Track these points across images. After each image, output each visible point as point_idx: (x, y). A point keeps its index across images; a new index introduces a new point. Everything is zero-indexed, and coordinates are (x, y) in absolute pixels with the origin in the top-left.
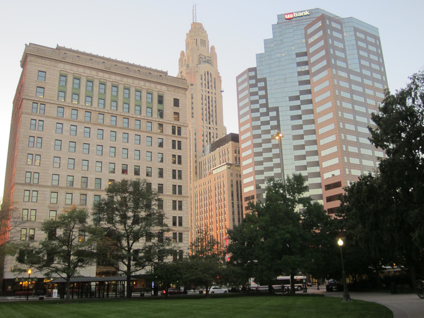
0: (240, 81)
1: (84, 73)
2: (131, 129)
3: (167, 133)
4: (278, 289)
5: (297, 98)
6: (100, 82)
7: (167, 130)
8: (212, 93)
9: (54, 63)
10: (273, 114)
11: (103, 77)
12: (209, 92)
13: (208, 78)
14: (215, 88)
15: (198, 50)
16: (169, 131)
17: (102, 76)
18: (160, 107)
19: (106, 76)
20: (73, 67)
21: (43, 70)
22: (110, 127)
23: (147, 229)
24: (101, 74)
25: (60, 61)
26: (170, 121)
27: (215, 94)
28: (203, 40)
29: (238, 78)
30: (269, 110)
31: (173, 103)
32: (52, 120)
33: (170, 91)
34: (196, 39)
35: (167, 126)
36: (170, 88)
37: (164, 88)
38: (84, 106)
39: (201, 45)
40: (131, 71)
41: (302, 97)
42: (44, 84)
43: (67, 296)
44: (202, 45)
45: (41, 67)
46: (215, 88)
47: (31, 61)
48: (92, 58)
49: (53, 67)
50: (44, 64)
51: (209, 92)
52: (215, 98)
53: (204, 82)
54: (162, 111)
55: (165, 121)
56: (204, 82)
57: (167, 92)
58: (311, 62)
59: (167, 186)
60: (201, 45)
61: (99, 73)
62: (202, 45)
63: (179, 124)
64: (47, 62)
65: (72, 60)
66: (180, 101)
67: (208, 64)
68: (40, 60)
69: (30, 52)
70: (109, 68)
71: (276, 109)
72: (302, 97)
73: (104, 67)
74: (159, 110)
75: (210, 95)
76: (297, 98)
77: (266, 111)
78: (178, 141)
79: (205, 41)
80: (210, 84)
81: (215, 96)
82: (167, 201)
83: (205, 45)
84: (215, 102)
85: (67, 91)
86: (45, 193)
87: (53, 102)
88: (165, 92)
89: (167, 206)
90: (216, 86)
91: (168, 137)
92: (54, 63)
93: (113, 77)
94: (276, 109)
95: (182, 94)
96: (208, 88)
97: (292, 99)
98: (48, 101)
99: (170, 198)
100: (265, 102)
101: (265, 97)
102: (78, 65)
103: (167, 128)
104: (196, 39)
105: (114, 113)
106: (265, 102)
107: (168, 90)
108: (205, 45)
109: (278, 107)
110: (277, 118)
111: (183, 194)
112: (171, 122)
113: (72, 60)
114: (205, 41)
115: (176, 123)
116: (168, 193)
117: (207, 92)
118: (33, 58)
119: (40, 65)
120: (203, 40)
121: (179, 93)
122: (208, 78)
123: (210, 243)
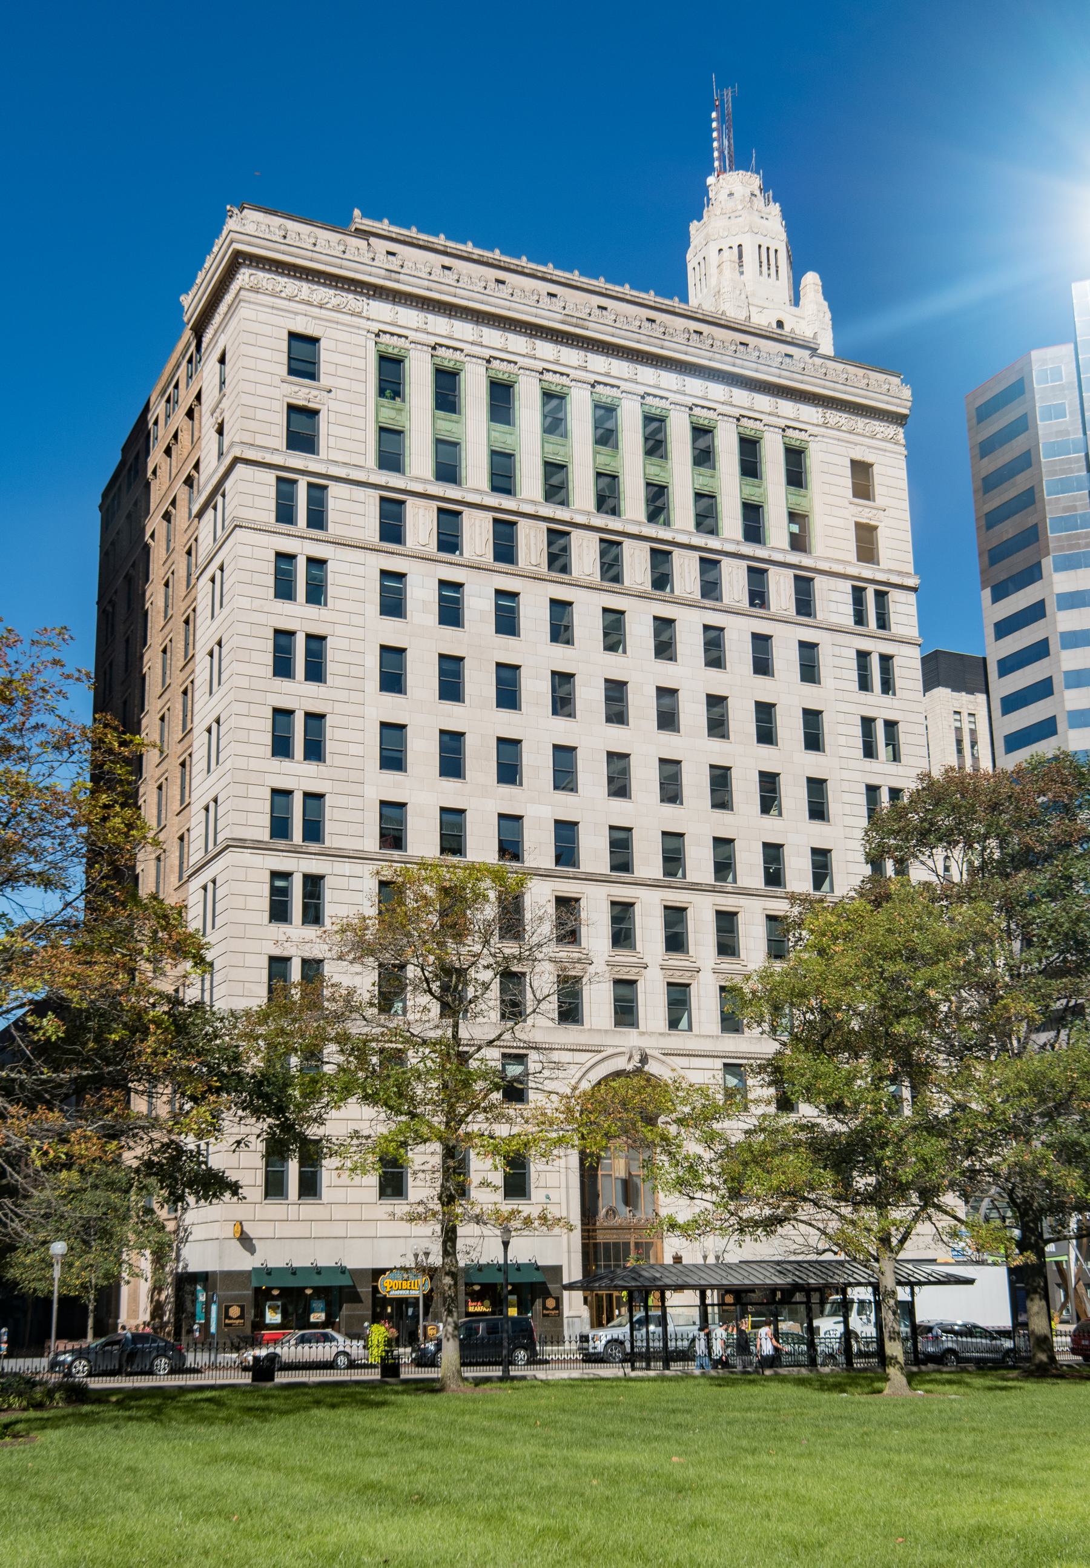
9: (350, 300)
17: (444, 333)
20: (283, 280)
23: (928, 1056)
26: (900, 573)
36: (835, 417)
37: (810, 413)
42: (315, 392)
48: (448, 261)
49: (349, 318)
50: (309, 303)
54: (615, 477)
57: (823, 430)
63: (313, 467)
64: (323, 293)
65: (559, 317)
66: (876, 469)
68: (290, 285)
69: (563, 322)
70: (581, 322)
74: (698, 496)
78: (312, 561)
85: (413, 427)
86: (355, 884)
99: (370, 868)
104: (740, 246)
107: (825, 425)
115: (298, 460)
118: (262, 277)
119: (294, 306)
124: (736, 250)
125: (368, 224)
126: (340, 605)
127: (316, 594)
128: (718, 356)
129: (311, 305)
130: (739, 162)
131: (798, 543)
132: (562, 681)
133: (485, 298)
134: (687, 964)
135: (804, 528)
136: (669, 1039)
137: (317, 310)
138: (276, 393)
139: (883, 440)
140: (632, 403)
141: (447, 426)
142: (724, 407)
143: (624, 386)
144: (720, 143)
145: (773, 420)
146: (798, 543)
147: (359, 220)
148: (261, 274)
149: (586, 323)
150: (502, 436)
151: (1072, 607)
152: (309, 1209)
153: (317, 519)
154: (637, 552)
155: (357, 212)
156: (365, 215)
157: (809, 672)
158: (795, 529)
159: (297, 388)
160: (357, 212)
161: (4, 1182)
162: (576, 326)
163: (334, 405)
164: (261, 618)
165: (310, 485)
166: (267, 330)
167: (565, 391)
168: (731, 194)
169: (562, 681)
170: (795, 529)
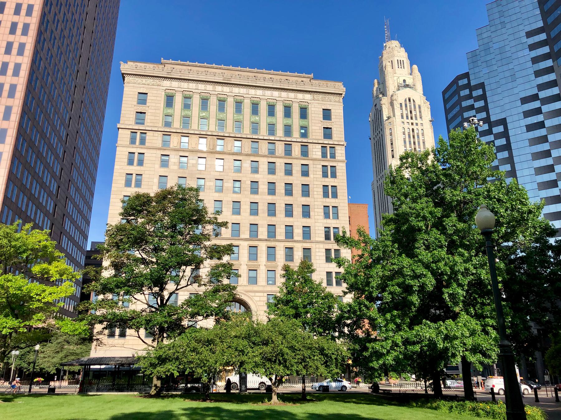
0: (447, 96)
2: (262, 155)
5: (535, 97)
6: (219, 98)
9: (157, 81)
10: (499, 129)
11: (222, 91)
12: (412, 124)
13: (410, 106)
14: (421, 118)
15: (395, 73)
18: (304, 122)
19: (226, 89)
20: (182, 84)
21: (144, 92)
22: (233, 154)
24: (219, 88)
25: (165, 78)
29: (444, 93)
30: (492, 125)
31: (322, 116)
32: (154, 151)
33: (316, 100)
36: (316, 96)
37: (308, 97)
38: (196, 130)
39: (398, 67)
40: (260, 80)
41: (543, 94)
42: (144, 108)
43: (194, 393)
44: (400, 67)
46: (421, 118)
47: (129, 83)
51: (412, 124)
52: (422, 129)
53: (405, 112)
55: (311, 141)
56: (405, 112)
58: (555, 51)
59: (317, 228)
60: (398, 67)
61: (217, 87)
62: (400, 67)
64: (150, 81)
67: (408, 89)
69: (223, 80)
70: (228, 80)
71: (503, 122)
72: (543, 94)
74: (302, 128)
75: (415, 127)
76: (535, 97)
77: (505, 143)
80: (414, 113)
83: (404, 66)
84: (423, 134)
88: (309, 102)
90: (423, 115)
91: (316, 162)
92: (158, 81)
93: (236, 90)
94: (503, 122)
95: (335, 102)
97: (524, 101)
100: (503, 130)
101: (485, 109)
103: (314, 150)
105: (237, 136)
106: (503, 130)
108: (404, 66)
109: (505, 119)
110: (505, 134)
111: (147, 144)
112: (320, 142)
116: (318, 239)
117: (410, 124)
122: (410, 106)
124: (391, 62)
126: (147, 165)
127: (141, 163)
129: (145, 85)
130: (392, 38)
131: (304, 135)
134: (256, 263)
136: (249, 287)
138: (133, 109)
139: (335, 102)
140: (247, 100)
141: (288, 121)
142: (230, 94)
144: (387, 33)
145: (196, 91)
146: (304, 135)
147: (163, 61)
150: (271, 120)
151: (5, 111)
152: (122, 341)
157: (305, 173)
160: (162, 58)
161: (522, 378)
163: (150, 111)
164: (122, 171)
166: (132, 93)
167: (225, 99)
168: (389, 47)
170: (303, 131)
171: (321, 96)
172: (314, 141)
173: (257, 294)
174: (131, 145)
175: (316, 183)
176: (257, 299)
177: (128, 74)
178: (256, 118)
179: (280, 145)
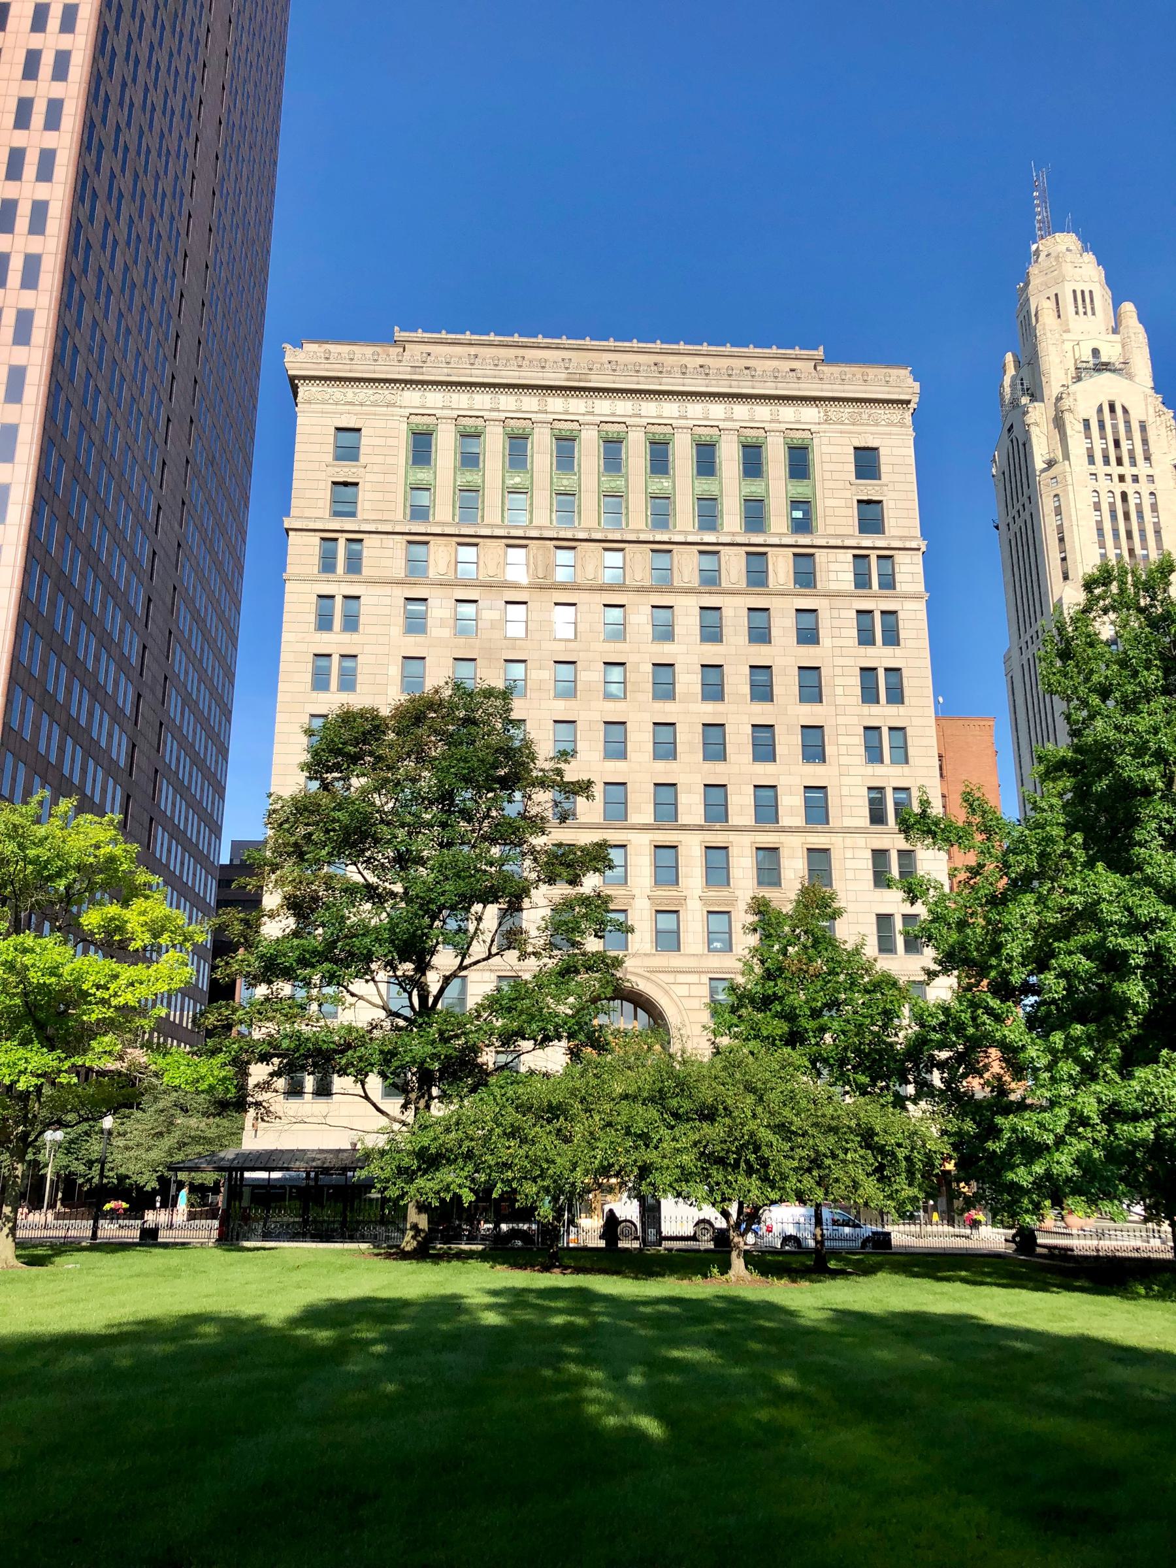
1: (680, 418)
2: (682, 588)
3: (834, 586)
4: (263, 1179)
7: (832, 576)
8: (1136, 479)
14: (1147, 458)
15: (1067, 331)
16: (841, 576)
18: (800, 489)
19: (577, 405)
20: (455, 396)
24: (556, 404)
25: (406, 382)
27: (1151, 478)
28: (1083, 292)
32: (387, 589)
33: (835, 423)
34: (1056, 295)
35: (832, 557)
36: (834, 411)
37: (810, 414)
38: (498, 526)
39: (1077, 313)
44: (1081, 310)
45: (342, 414)
46: (1147, 458)
52: (1152, 494)
60: (1077, 313)
62: (1081, 310)
66: (882, 451)
67: (1108, 374)
69: (568, 380)
73: (563, 376)
79: (1091, 292)
80: (1125, 446)
81: (1152, 488)
82: (849, 854)
83: (1093, 309)
87: (389, 529)
88: (814, 428)
89: (850, 875)
91: (838, 602)
92: (387, 392)
93: (604, 406)
96: (1119, 462)
98: (372, 528)
99: (860, 840)
102: (471, 384)
104: (1056, 295)
108: (1093, 309)
113: (446, 370)
114: (1091, 292)
116: (848, 822)
120: (1083, 292)
121: (877, 425)
123: (301, 856)
124: (1053, 299)
125: (405, 335)
127: (351, 623)
128: (714, 382)
131: (803, 526)
132: (712, 670)
133: (497, 373)
134: (675, 893)
135: (807, 513)
137: (359, 408)
138: (323, 476)
141: (755, 488)
142: (539, 415)
143: (438, 413)
144: (1041, 213)
147: (399, 335)
148: (314, 389)
149: (589, 377)
150: (706, 486)
152: (321, 1106)
153: (354, 564)
154: (733, 558)
155: (396, 328)
156: (402, 330)
157: (808, 635)
158: (798, 514)
159: (338, 470)
160: (396, 328)
162: (580, 381)
163: (369, 477)
165: (879, 557)
168: (1048, 255)
169: (712, 670)
170: (798, 514)
171: (847, 411)
172: (832, 542)
173: (682, 978)
174: (325, 576)
175: (839, 661)
176: (682, 991)
177: (305, 378)
178: (662, 484)
179: (733, 558)
